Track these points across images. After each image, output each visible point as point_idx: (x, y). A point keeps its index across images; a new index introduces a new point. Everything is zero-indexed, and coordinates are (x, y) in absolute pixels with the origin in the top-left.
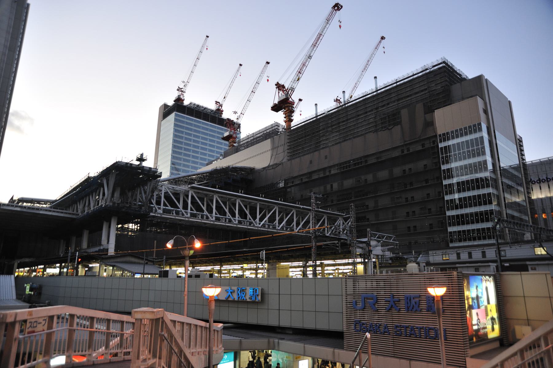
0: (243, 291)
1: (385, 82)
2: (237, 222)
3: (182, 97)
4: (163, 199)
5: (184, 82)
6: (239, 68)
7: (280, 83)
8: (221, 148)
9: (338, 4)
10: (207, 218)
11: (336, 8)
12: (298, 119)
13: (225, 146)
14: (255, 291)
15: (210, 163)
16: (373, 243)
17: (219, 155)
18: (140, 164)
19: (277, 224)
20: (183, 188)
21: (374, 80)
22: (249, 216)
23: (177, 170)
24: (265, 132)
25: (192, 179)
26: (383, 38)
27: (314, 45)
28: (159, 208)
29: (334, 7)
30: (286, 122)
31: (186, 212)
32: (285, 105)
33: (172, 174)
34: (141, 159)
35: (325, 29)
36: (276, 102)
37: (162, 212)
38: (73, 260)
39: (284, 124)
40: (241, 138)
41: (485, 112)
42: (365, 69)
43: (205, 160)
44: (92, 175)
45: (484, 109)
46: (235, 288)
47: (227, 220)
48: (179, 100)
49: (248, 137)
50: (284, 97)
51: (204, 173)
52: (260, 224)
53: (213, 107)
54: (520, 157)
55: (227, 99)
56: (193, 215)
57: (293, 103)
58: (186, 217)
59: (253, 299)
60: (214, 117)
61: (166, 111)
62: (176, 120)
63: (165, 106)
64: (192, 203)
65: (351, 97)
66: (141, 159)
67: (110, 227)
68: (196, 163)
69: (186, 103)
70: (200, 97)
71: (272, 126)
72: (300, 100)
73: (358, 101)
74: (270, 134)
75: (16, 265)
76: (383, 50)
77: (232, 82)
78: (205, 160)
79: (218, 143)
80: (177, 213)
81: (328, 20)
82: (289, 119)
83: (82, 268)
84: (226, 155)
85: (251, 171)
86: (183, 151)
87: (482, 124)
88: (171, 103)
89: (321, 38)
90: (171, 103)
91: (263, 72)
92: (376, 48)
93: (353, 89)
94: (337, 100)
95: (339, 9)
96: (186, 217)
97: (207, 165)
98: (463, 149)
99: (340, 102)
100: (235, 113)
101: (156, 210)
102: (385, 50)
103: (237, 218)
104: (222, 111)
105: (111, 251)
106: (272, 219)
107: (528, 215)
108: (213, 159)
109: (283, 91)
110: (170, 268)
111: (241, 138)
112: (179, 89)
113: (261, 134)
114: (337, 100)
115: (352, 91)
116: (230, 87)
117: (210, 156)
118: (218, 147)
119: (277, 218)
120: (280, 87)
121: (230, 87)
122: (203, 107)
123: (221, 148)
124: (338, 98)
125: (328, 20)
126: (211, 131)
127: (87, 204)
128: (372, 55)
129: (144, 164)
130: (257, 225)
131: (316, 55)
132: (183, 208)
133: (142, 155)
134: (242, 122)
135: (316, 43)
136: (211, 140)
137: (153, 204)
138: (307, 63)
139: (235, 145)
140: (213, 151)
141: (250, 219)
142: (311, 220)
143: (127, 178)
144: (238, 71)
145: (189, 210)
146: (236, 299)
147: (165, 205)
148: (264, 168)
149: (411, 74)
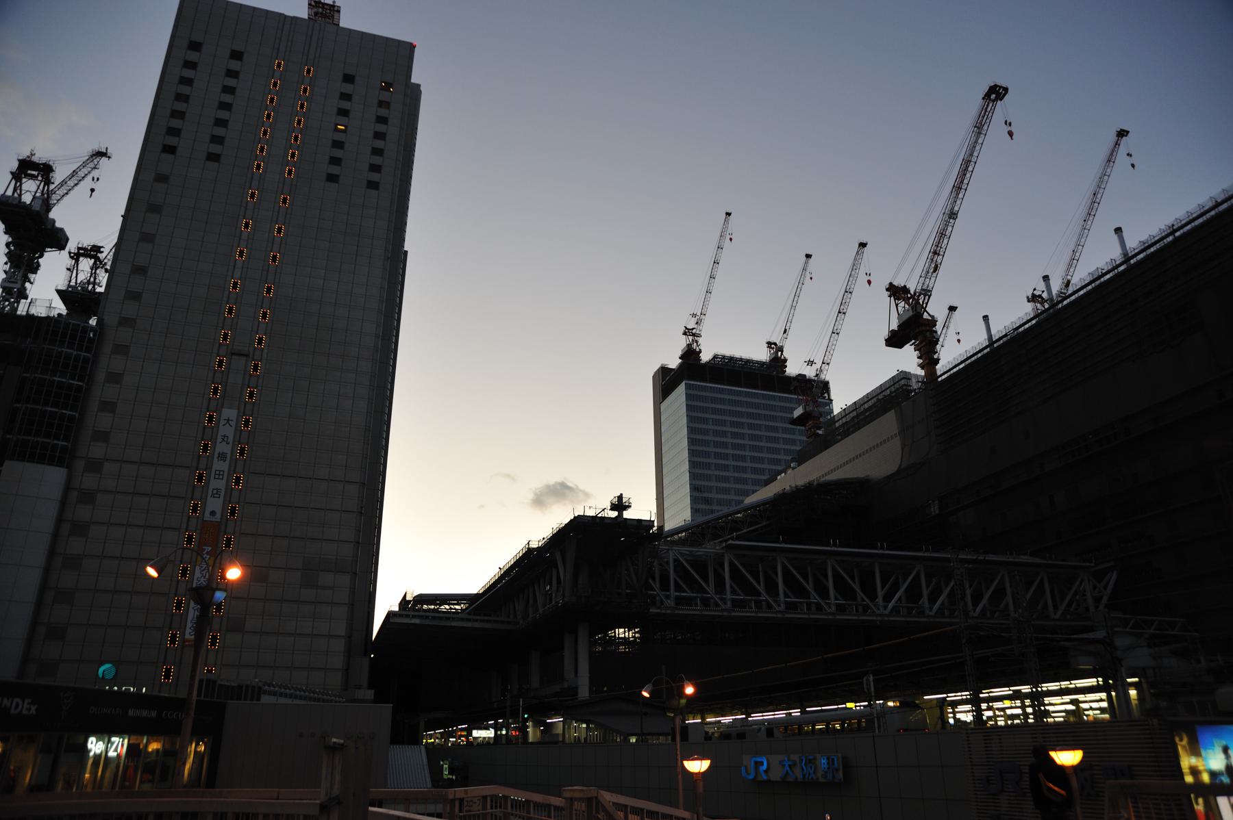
0: (810, 762)
1: (1144, 238)
2: (833, 609)
3: (694, 346)
4: (672, 576)
5: (694, 315)
6: (806, 263)
7: (895, 283)
8: (793, 442)
9: (996, 86)
10: (770, 607)
11: (993, 96)
12: (950, 355)
13: (800, 436)
14: (831, 762)
15: (773, 479)
16: (1120, 642)
18: (620, 515)
19: (927, 605)
20: (710, 548)
23: (708, 501)
24: (881, 397)
25: (734, 521)
27: (958, 188)
28: (668, 597)
29: (987, 96)
31: (722, 599)
32: (915, 330)
33: (694, 511)
34: (620, 505)
35: (978, 148)
36: (894, 326)
37: (673, 604)
38: (515, 714)
39: (922, 373)
40: (837, 408)
42: (1090, 214)
43: (762, 471)
44: (534, 545)
46: (795, 757)
47: (813, 607)
48: (690, 355)
49: (845, 412)
50: (911, 313)
51: (759, 506)
52: (886, 608)
53: (762, 355)
55: (790, 333)
56: (737, 604)
57: (933, 322)
58: (723, 610)
59: (830, 776)
60: (771, 374)
61: (665, 381)
62: (688, 397)
63: (664, 371)
64: (732, 578)
65: (1068, 284)
66: (620, 505)
67: (576, 642)
68: (744, 481)
69: (705, 357)
70: (735, 338)
71: (894, 381)
72: (952, 309)
73: (1082, 293)
74: (892, 396)
75: (422, 725)
76: (1129, 161)
77: (797, 295)
78: (762, 471)
79: (785, 430)
80: (706, 602)
81: (979, 127)
82: (929, 359)
83: (534, 726)
84: (802, 458)
85: (860, 486)
86: (746, 431)
88: (674, 362)
89: (970, 169)
90: (674, 362)
91: (854, 267)
92: (1109, 161)
93: (1070, 265)
95: (1000, 97)
96: (723, 610)
97: (767, 483)
99: (1043, 301)
100: (810, 363)
101: (662, 602)
102: (1134, 160)
103: (833, 601)
104: (785, 360)
105: (584, 693)
106: (913, 594)
108: (780, 468)
109: (906, 300)
110: (703, 718)
111: (837, 408)
112: (687, 332)
113: (870, 403)
115: (1068, 270)
116: (793, 307)
117: (771, 461)
118: (786, 441)
119: (925, 592)
120: (896, 292)
121: (793, 307)
122: (741, 359)
123: (793, 442)
124: (1037, 293)
125: (979, 127)
126: (766, 407)
127: (531, 602)
128: (1103, 178)
129: (627, 514)
131: (966, 209)
132: (716, 593)
133: (620, 497)
134: (827, 376)
135: (962, 182)
136: (768, 428)
137: (653, 589)
138: (950, 229)
139: (820, 432)
140: (777, 451)
142: (1008, 585)
143: (591, 549)
144: (804, 269)
145: (729, 596)
146: (800, 778)
147: (678, 588)
148: (889, 477)
149: (1210, 205)
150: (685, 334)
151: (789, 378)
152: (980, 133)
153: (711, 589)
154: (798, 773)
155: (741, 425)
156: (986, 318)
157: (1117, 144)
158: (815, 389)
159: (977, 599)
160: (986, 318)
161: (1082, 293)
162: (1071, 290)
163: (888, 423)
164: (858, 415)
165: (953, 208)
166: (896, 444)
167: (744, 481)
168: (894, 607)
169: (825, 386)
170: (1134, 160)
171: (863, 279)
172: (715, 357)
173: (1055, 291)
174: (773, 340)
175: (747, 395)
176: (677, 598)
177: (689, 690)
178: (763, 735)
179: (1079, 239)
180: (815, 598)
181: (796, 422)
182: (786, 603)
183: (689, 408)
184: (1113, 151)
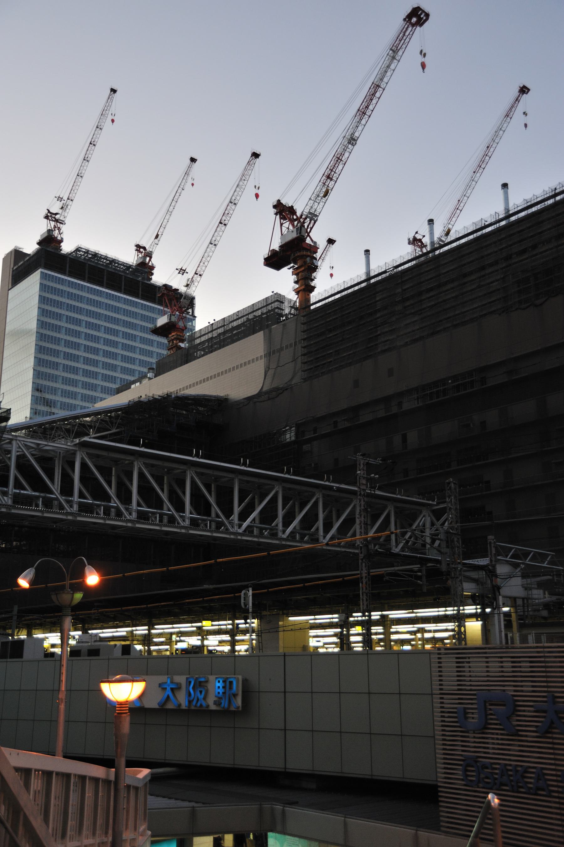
0: (201, 685)
2: (187, 522)
3: (56, 233)
5: (60, 199)
6: (189, 167)
7: (283, 202)
8: (150, 354)
10: (119, 514)
11: (414, 20)
12: (327, 284)
13: (160, 347)
14: (227, 684)
15: (126, 386)
16: (502, 569)
17: (146, 370)
19: (280, 527)
23: (48, 403)
24: (251, 317)
25: (83, 425)
29: (409, 17)
31: (68, 502)
32: (295, 254)
33: (35, 412)
35: (389, 74)
36: (276, 246)
37: (10, 502)
40: (197, 329)
42: (481, 166)
43: (113, 379)
46: (181, 679)
48: (50, 242)
49: (212, 328)
50: (294, 235)
51: (110, 411)
52: (240, 526)
53: (130, 258)
55: (162, 239)
58: (68, 514)
59: (225, 703)
60: (134, 280)
62: (43, 287)
63: (17, 254)
65: (448, 233)
68: (93, 387)
69: (67, 248)
71: (267, 302)
72: (331, 242)
74: (261, 319)
76: (524, 120)
77: (174, 200)
78: (113, 379)
79: (143, 340)
80: (48, 504)
81: (395, 51)
82: (305, 286)
84: (161, 368)
85: (220, 404)
89: (378, 95)
91: (243, 177)
92: (507, 116)
94: (415, 239)
95: (420, 23)
96: (68, 514)
97: (119, 391)
99: (423, 246)
100: (182, 271)
102: (528, 120)
103: (187, 514)
104: (152, 268)
106: (268, 516)
108: (132, 379)
109: (292, 221)
113: (240, 322)
114: (415, 239)
116: (169, 212)
118: (143, 352)
119: (281, 513)
120: (283, 211)
121: (169, 212)
122: (106, 258)
123: (150, 354)
124: (418, 237)
125: (395, 51)
132: (62, 493)
135: (367, 107)
138: (347, 154)
139: (182, 345)
141: (218, 516)
144: (187, 173)
145: (76, 498)
146: (184, 704)
150: (47, 217)
151: (154, 287)
152: (394, 58)
153: (56, 487)
154: (182, 699)
155: (97, 327)
156: (367, 252)
157: (517, 100)
158: (179, 302)
159: (328, 527)
160: (367, 252)
161: (463, 241)
162: (450, 239)
163: (256, 344)
164: (224, 333)
165: (353, 134)
166: (260, 366)
167: (93, 387)
168: (249, 527)
169: (191, 302)
170: (528, 120)
171: (250, 191)
172: (78, 250)
173: (437, 235)
174: (142, 244)
175: (108, 296)
176: (15, 496)
177: (93, 579)
178: (118, 653)
179: (466, 190)
180: (168, 508)
181: (158, 331)
182: (139, 512)
183: (42, 300)
184: (512, 107)
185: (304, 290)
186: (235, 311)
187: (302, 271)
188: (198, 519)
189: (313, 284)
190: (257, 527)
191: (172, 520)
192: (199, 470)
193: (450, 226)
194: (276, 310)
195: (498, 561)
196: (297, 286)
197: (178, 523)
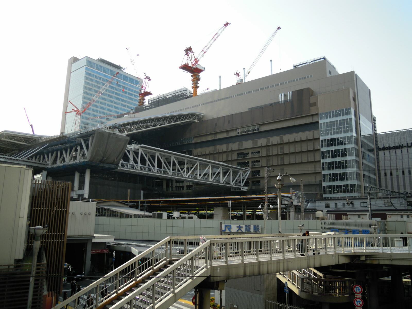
2: (139, 168)
17: (130, 110)
21: (270, 62)
22: (148, 162)
24: (174, 95)
26: (279, 28)
30: (193, 88)
41: (354, 99)
45: (353, 98)
52: (187, 175)
54: (373, 121)
87: (352, 108)
94: (237, 73)
98: (336, 126)
107: (375, 165)
108: (124, 112)
114: (237, 73)
117: (122, 109)
124: (238, 72)
130: (186, 175)
141: (149, 166)
185: (195, 87)
186: (168, 92)
187: (195, 80)
188: (124, 163)
189: (198, 85)
190: (147, 168)
191: (149, 170)
192: (160, 153)
193: (250, 71)
194: (184, 94)
195: (292, 195)
196: (192, 85)
197: (135, 168)
